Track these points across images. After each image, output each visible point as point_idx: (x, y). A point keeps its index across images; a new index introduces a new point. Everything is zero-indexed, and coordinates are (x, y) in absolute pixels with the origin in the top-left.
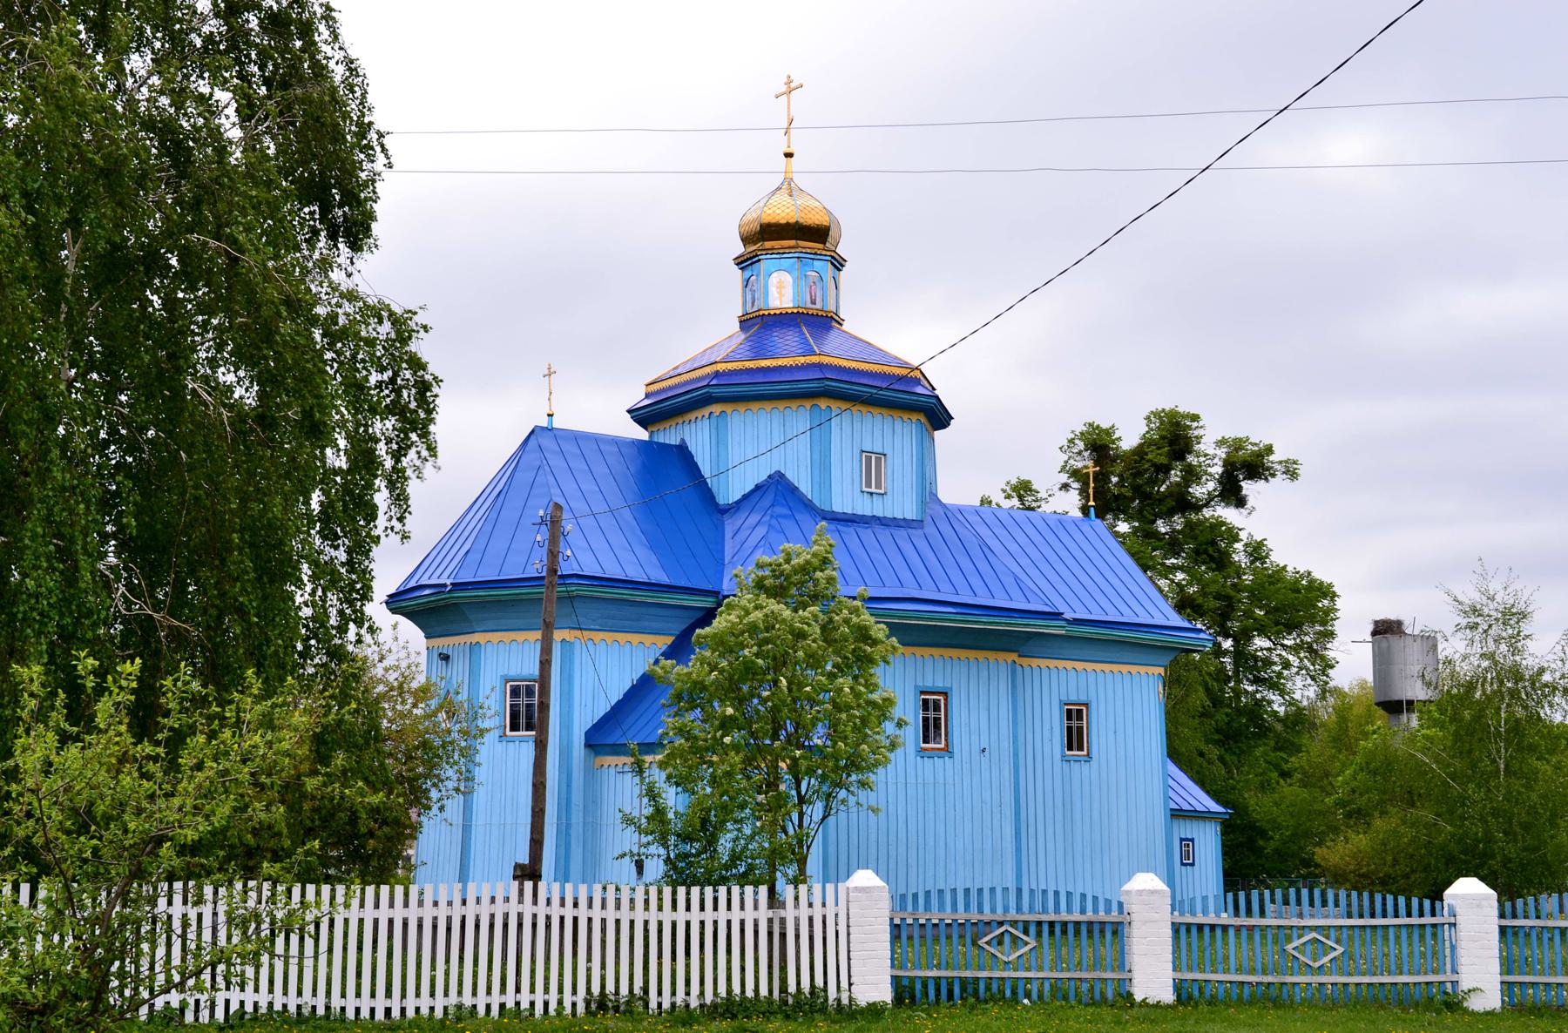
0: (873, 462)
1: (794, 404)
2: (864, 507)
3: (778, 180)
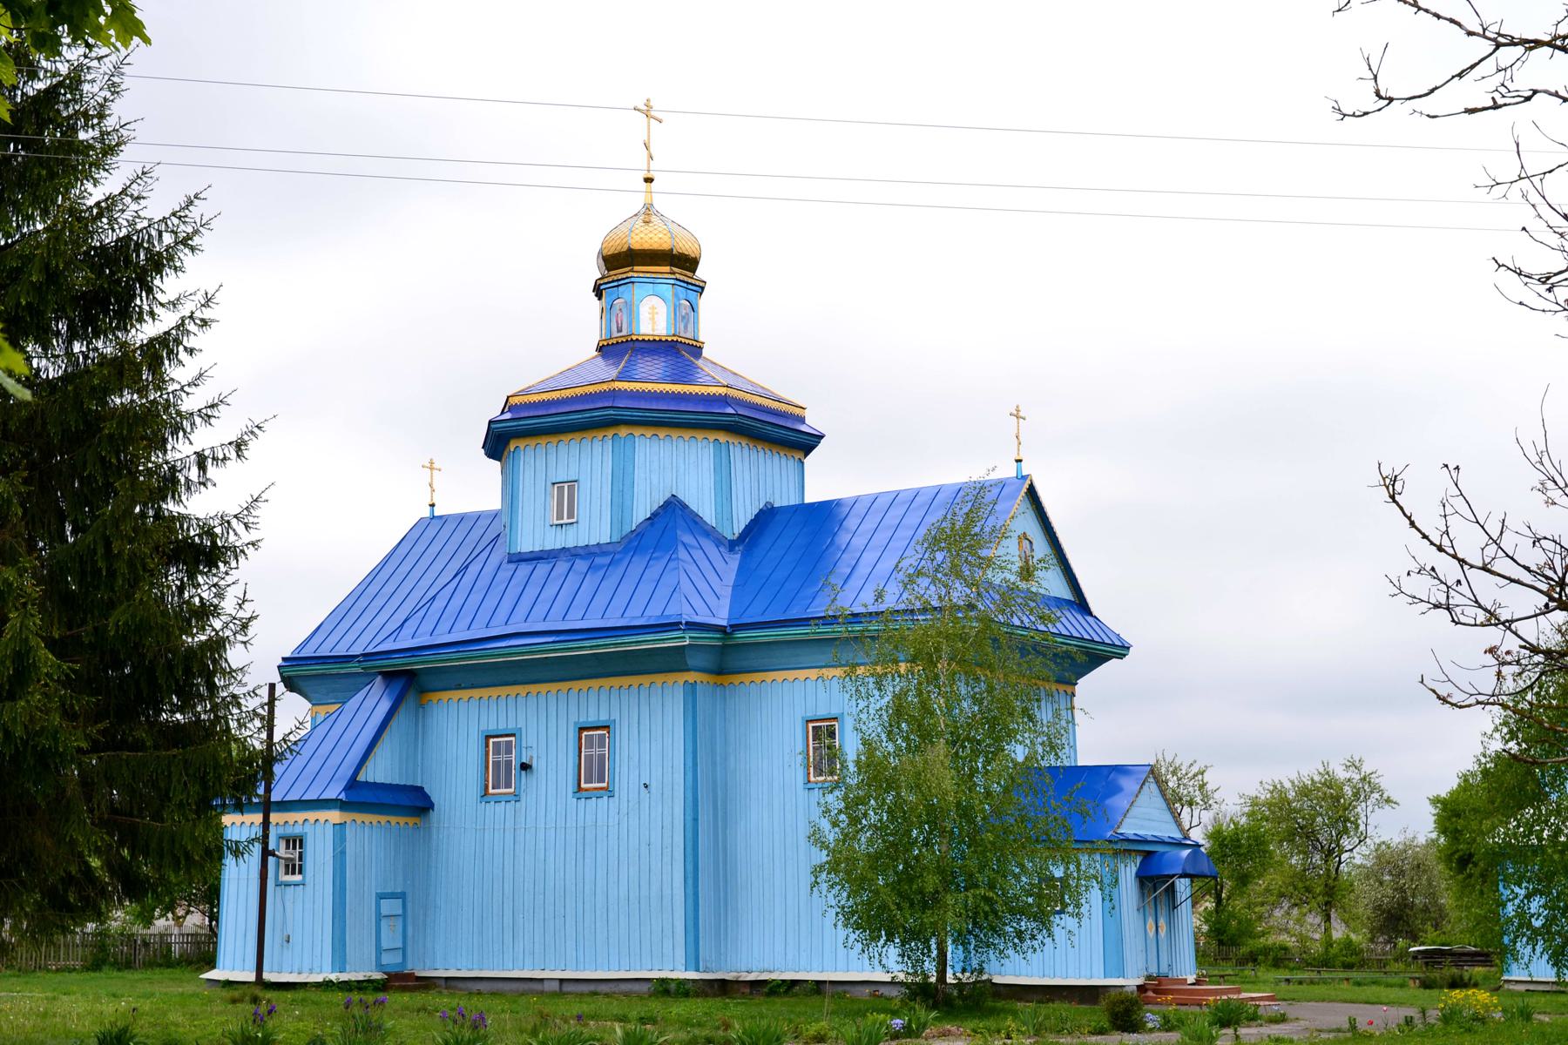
0: (567, 489)
1: (700, 435)
2: (554, 540)
3: (638, 206)
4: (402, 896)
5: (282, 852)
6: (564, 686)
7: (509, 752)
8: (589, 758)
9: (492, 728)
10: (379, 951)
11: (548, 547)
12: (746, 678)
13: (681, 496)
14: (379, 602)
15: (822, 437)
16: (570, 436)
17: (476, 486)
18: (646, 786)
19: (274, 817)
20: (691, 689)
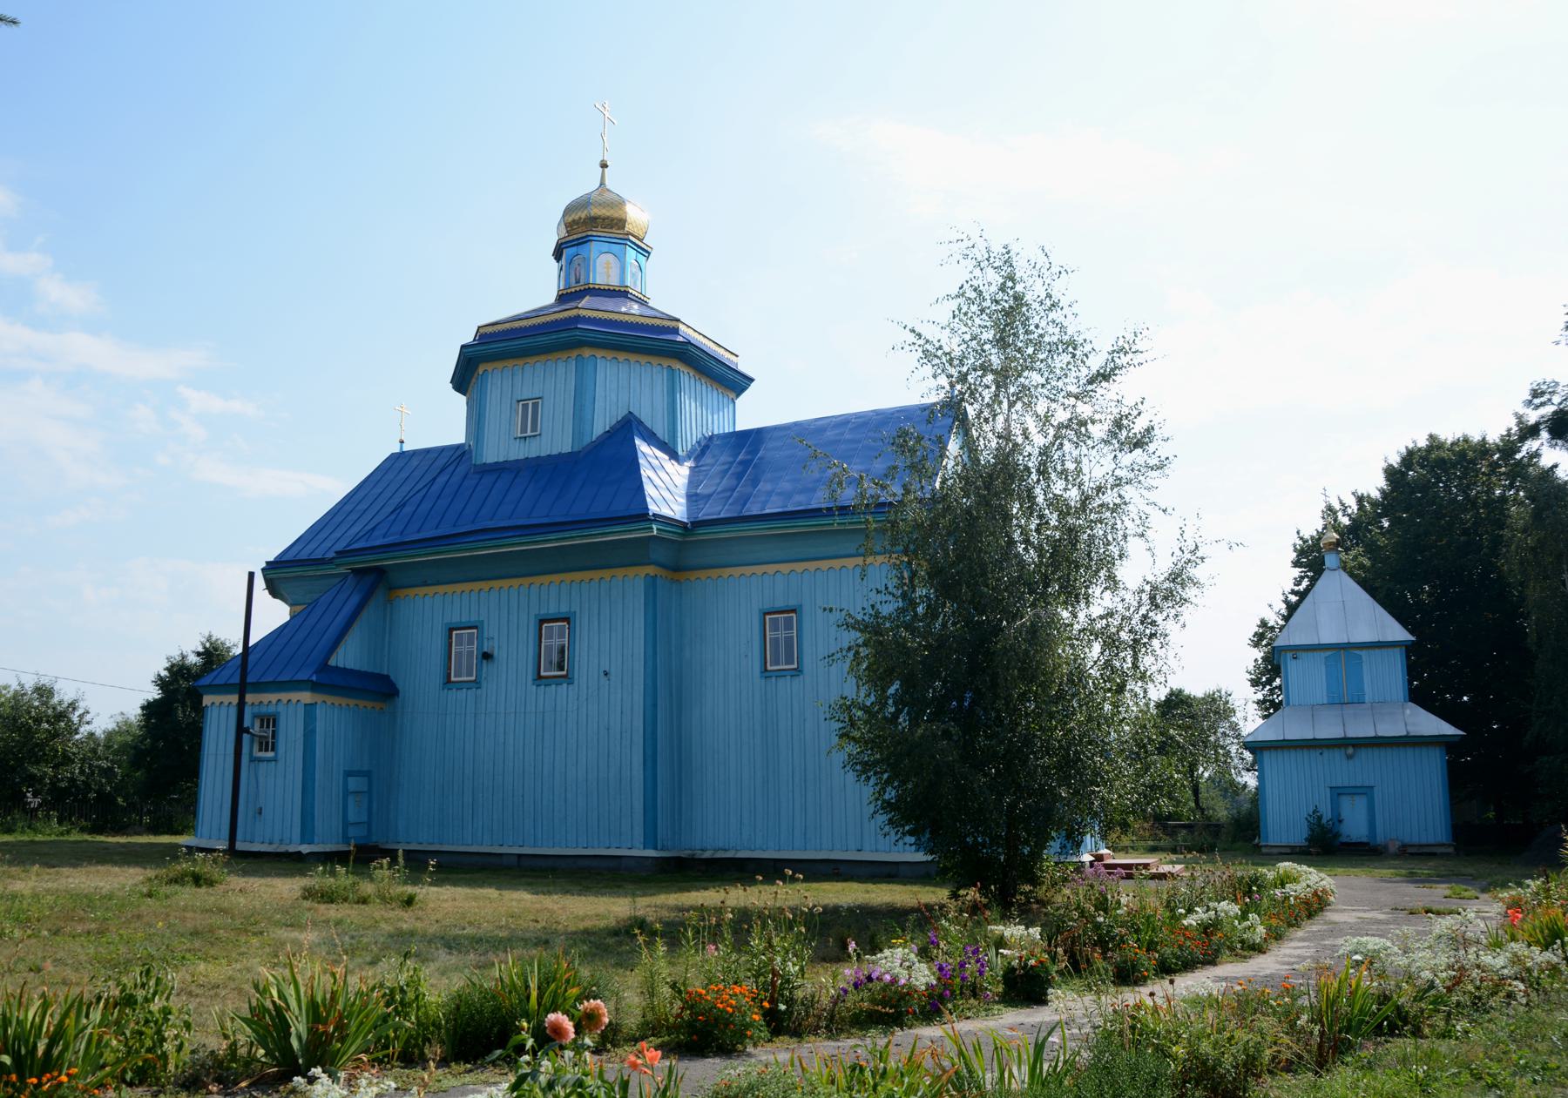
0: (531, 409)
1: (655, 360)
4: (368, 774)
5: (256, 729)
6: (526, 581)
7: (788, 626)
8: (775, 641)
9: (456, 619)
10: (346, 824)
11: (512, 458)
12: (703, 574)
13: (636, 413)
14: (353, 517)
15: (752, 380)
16: (536, 358)
17: (442, 421)
18: (606, 674)
19: (249, 698)
20: (652, 581)
